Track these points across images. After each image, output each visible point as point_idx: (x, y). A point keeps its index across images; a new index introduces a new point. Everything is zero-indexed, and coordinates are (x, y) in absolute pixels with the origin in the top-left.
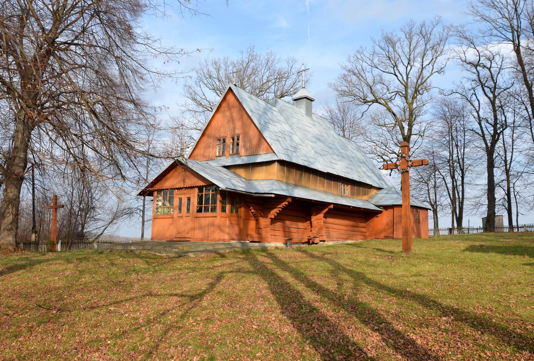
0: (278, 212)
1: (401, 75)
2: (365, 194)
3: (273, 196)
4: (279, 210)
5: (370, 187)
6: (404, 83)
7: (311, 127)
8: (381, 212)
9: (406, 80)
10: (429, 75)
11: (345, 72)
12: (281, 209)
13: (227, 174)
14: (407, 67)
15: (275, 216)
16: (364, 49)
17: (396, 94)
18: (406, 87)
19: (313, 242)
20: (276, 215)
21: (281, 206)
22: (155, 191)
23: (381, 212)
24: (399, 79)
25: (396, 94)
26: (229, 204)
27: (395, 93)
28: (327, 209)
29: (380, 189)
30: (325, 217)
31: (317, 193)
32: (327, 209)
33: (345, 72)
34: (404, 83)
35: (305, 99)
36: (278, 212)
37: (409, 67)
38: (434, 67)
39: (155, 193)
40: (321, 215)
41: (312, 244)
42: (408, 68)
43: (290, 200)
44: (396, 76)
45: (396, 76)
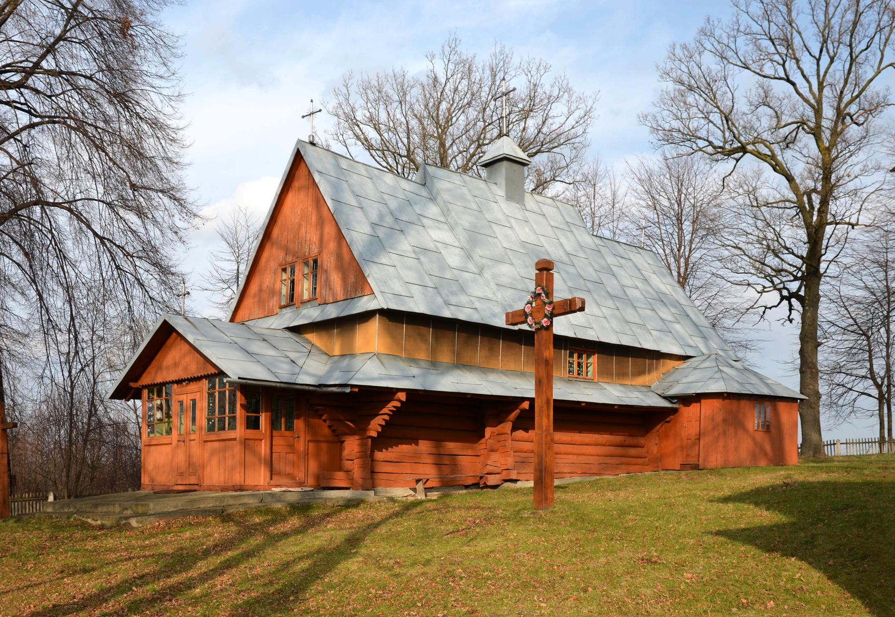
0: (383, 423)
1: (808, 81)
2: (640, 372)
3: (348, 390)
4: (384, 420)
5: (658, 355)
6: (813, 101)
7: (511, 227)
8: (674, 411)
9: (817, 93)
10: (873, 74)
11: (374, 82)
12: (387, 417)
13: (292, 346)
14: (818, 60)
15: (378, 432)
16: (716, 23)
17: (798, 127)
18: (818, 112)
19: (485, 483)
20: (380, 429)
21: (385, 410)
22: (145, 387)
23: (674, 411)
24: (801, 91)
25: (798, 127)
26: (266, 411)
27: (795, 126)
28: (517, 411)
29: (686, 358)
30: (514, 429)
31: (504, 379)
32: (517, 411)
33: (374, 82)
34: (813, 101)
35: (505, 163)
36: (383, 423)
37: (825, 60)
38: (885, 53)
39: (145, 392)
40: (507, 426)
41: (482, 488)
42: (821, 62)
43: (402, 396)
44: (793, 84)
45: (793, 84)
